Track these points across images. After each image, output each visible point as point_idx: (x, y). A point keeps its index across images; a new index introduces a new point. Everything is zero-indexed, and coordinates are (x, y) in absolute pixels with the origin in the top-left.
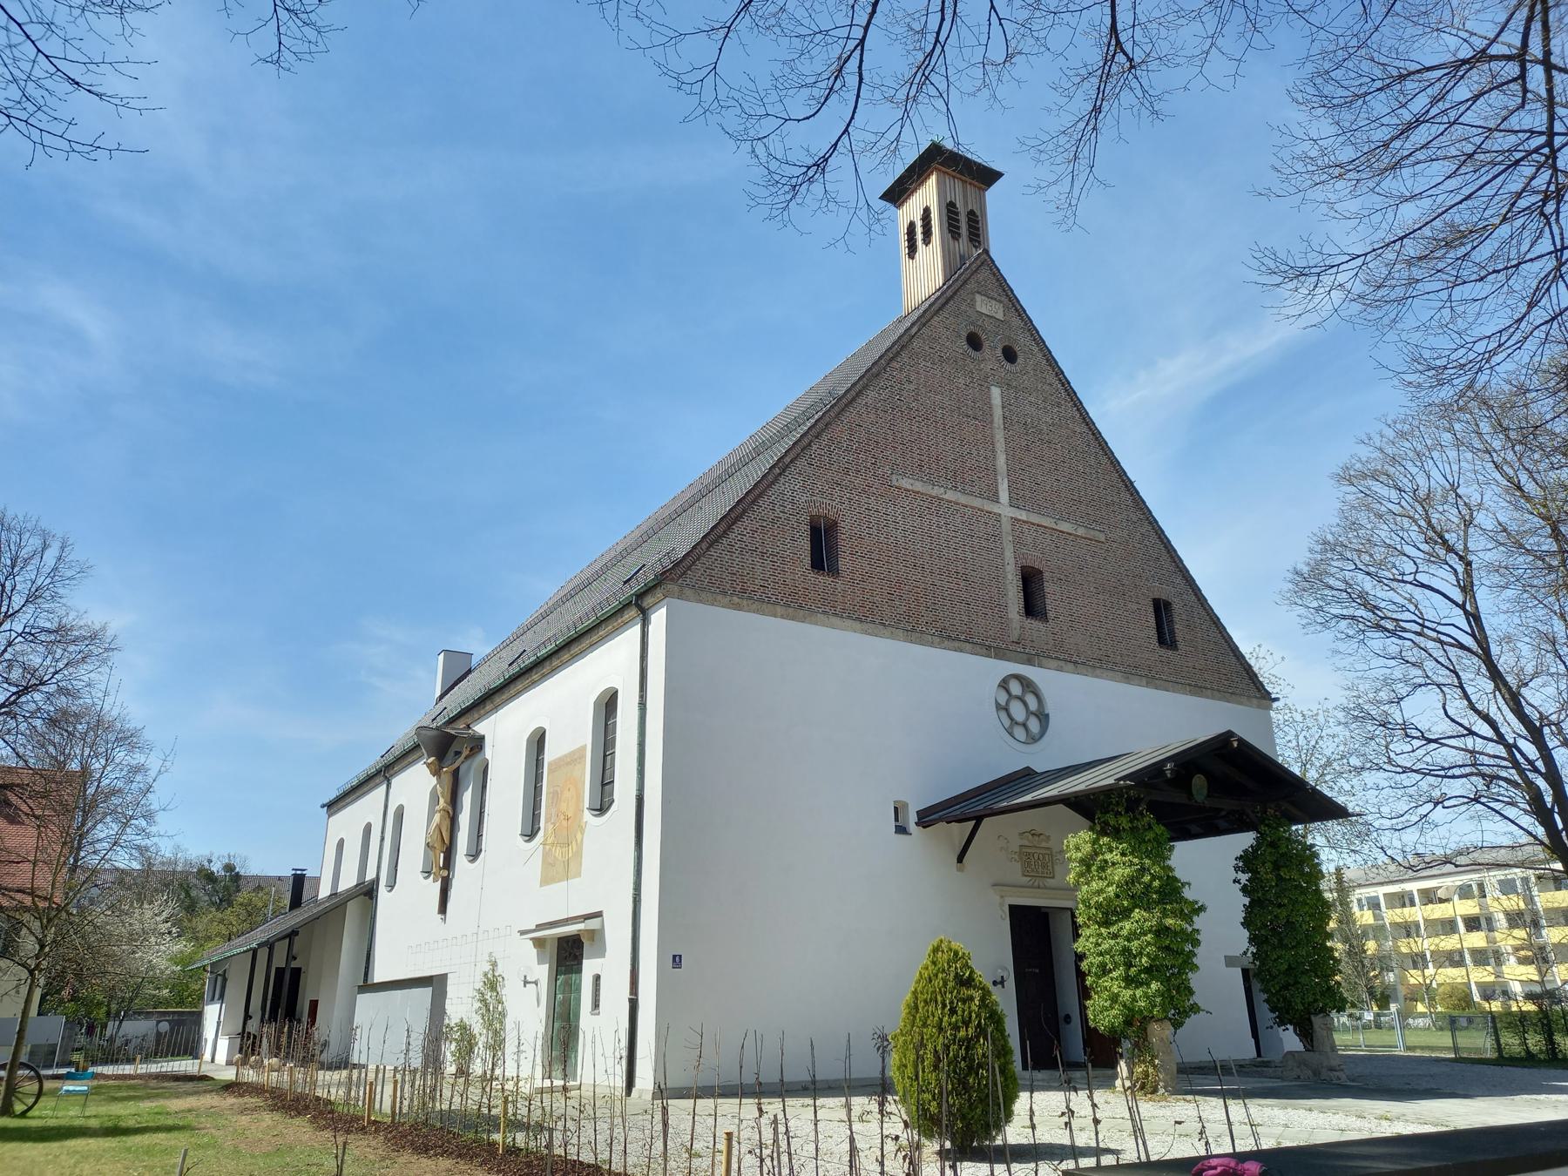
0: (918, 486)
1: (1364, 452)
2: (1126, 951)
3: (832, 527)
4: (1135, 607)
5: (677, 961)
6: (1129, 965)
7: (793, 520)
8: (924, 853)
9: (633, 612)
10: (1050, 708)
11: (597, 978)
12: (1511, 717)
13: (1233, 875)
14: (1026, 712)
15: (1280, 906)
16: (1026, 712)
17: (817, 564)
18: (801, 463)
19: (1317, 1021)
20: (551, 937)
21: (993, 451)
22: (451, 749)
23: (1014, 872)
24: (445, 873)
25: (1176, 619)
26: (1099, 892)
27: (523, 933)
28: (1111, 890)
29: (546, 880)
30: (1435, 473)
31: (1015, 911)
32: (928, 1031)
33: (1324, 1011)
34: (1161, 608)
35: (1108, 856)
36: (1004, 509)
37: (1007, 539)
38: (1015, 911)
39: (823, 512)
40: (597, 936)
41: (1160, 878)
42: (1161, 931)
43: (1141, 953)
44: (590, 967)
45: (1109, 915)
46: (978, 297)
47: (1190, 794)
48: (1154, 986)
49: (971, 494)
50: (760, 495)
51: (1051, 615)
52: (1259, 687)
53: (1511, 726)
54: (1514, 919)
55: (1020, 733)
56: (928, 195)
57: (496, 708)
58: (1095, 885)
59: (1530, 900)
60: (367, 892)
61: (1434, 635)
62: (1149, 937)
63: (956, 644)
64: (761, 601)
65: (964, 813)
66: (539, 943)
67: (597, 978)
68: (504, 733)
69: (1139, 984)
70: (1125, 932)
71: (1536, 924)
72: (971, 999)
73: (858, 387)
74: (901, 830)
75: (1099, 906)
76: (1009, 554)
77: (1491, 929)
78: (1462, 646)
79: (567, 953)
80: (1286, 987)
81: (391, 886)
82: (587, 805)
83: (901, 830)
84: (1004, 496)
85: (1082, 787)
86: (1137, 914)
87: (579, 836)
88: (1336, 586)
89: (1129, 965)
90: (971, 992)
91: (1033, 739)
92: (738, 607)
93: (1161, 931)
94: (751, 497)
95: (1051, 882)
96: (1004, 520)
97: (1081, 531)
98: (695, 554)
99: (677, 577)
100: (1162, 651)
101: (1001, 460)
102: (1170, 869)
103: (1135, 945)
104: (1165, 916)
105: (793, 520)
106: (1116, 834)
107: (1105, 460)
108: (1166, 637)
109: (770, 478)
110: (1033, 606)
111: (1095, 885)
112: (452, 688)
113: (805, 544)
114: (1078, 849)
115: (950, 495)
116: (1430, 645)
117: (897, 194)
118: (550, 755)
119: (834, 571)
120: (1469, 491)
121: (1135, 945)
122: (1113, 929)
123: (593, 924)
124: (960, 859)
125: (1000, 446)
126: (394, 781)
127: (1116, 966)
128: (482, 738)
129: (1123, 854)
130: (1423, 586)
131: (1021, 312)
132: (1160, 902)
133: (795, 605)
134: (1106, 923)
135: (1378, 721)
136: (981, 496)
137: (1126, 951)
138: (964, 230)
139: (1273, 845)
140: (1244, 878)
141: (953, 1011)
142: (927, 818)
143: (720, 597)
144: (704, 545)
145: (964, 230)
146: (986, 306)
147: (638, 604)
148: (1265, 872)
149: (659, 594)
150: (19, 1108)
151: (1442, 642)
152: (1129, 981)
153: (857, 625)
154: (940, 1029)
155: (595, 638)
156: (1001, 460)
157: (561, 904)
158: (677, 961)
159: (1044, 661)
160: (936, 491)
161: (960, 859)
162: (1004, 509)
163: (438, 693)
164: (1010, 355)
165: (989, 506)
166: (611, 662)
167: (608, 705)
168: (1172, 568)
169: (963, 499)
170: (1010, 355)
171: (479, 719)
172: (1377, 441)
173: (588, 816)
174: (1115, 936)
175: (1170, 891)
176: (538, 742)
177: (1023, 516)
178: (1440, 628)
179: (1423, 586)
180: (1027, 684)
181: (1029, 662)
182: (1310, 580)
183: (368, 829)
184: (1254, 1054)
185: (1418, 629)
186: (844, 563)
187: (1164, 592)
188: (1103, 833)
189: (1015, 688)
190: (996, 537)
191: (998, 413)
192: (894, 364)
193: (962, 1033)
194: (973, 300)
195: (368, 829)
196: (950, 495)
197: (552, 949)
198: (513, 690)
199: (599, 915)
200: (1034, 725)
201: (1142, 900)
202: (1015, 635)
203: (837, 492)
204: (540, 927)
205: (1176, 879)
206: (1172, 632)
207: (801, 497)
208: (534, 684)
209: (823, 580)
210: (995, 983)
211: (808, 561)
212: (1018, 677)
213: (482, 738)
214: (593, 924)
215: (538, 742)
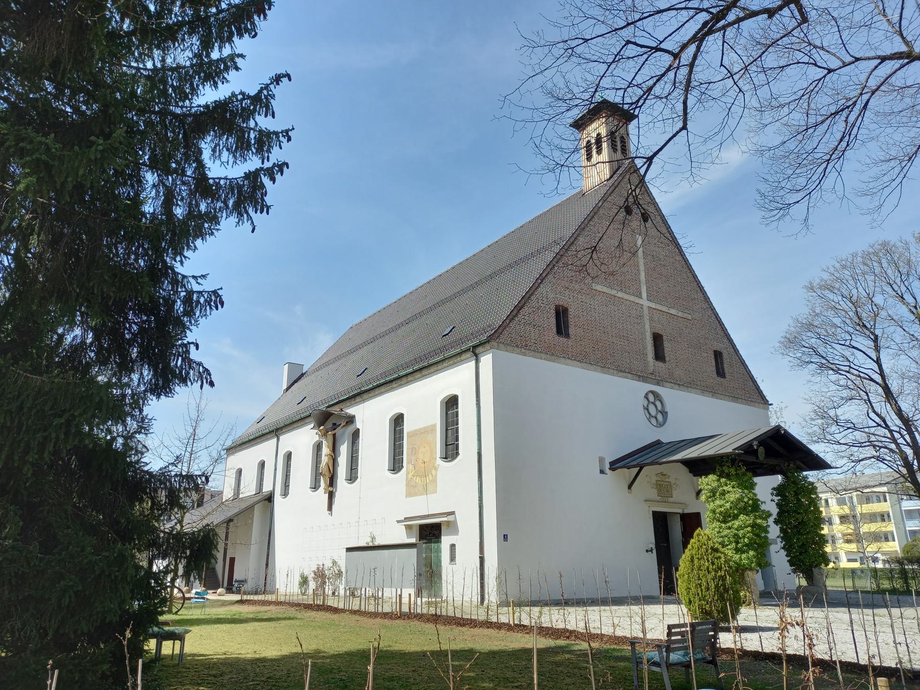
0: (605, 289)
1: (826, 276)
2: (736, 535)
3: (565, 310)
4: (705, 355)
5: (505, 537)
6: (737, 543)
7: (547, 307)
9: (469, 354)
10: (668, 409)
11: (453, 546)
12: (895, 417)
13: (771, 497)
14: (657, 412)
15: (799, 513)
16: (657, 412)
17: (559, 332)
18: (550, 277)
19: (815, 570)
20: (416, 525)
22: (332, 421)
23: (653, 494)
24: (331, 489)
25: (725, 362)
26: (721, 506)
27: (398, 522)
28: (728, 505)
29: (409, 495)
30: (861, 289)
31: (655, 514)
32: (702, 573)
33: (818, 565)
34: (718, 355)
35: (725, 488)
36: (645, 302)
37: (646, 318)
38: (655, 514)
39: (561, 303)
40: (453, 527)
41: (752, 499)
42: (754, 525)
43: (744, 537)
44: (446, 541)
45: (726, 517)
47: (757, 457)
48: (751, 553)
49: (629, 293)
50: (532, 295)
51: (667, 359)
52: (763, 397)
53: (894, 422)
54: (843, 519)
55: (653, 421)
56: (599, 128)
57: (364, 401)
58: (718, 502)
59: (852, 508)
61: (856, 372)
62: (749, 529)
63: (625, 374)
64: (534, 351)
65: (633, 462)
66: (409, 528)
67: (453, 546)
68: (371, 416)
69: (743, 552)
70: (735, 526)
71: (856, 522)
72: (720, 558)
73: (575, 235)
74: (602, 472)
75: (721, 513)
76: (647, 327)
77: (831, 524)
78: (872, 380)
79: (430, 533)
80: (801, 554)
81: (285, 494)
82: (438, 455)
83: (602, 472)
84: (644, 295)
85: (711, 452)
86: (742, 517)
87: (434, 472)
88: (807, 345)
89: (737, 543)
90: (719, 554)
91: (661, 425)
92: (524, 354)
93: (754, 525)
94: (528, 295)
95: (670, 500)
96: (645, 308)
97: (680, 314)
98: (503, 327)
100: (719, 379)
101: (643, 274)
102: (755, 495)
103: (741, 533)
104: (756, 518)
105: (547, 307)
106: (728, 476)
107: (690, 275)
108: (720, 373)
109: (536, 285)
110: (659, 355)
111: (718, 502)
112: (296, 382)
113: (553, 321)
114: (708, 484)
115: (620, 294)
116: (853, 377)
117: (580, 125)
118: (407, 427)
119: (567, 336)
120: (878, 299)
121: (741, 533)
122: (730, 524)
123: (451, 518)
124: (630, 487)
125: (642, 268)
126: (281, 438)
127: (731, 543)
128: (354, 417)
129: (733, 487)
130: (854, 347)
132: (752, 512)
133: (550, 353)
134: (725, 522)
135: (826, 417)
136: (633, 295)
137: (736, 535)
138: (619, 148)
139: (794, 482)
140: (776, 499)
141: (713, 564)
142: (614, 465)
143: (516, 349)
144: (508, 321)
145: (619, 148)
148: (790, 495)
149: (487, 346)
150: (174, 610)
151: (859, 376)
152: (737, 550)
153: (579, 364)
154: (709, 572)
155: (440, 367)
156: (643, 274)
157: (426, 507)
158: (505, 537)
159: (665, 384)
160: (613, 292)
161: (630, 487)
162: (645, 302)
163: (285, 387)
165: (637, 300)
166: (457, 379)
167: (451, 403)
168: (722, 334)
169: (626, 297)
171: (351, 406)
172: (832, 270)
173: (439, 462)
174: (730, 528)
175: (754, 507)
176: (398, 420)
177: (653, 305)
178: (860, 369)
179: (854, 347)
180: (656, 395)
181: (658, 384)
182: (791, 342)
183: (262, 465)
185: (847, 369)
186: (572, 331)
187: (719, 347)
188: (721, 476)
190: (641, 317)
192: (591, 223)
193: (719, 574)
195: (262, 465)
196: (620, 294)
197: (416, 531)
198: (377, 391)
199: (453, 513)
200: (660, 417)
201: (744, 510)
202: (651, 369)
203: (567, 293)
204: (407, 519)
205: (758, 500)
206: (723, 369)
207: (550, 295)
208: (393, 389)
209: (563, 340)
211: (555, 330)
212: (652, 392)
213: (354, 417)
214: (451, 518)
215: (398, 420)
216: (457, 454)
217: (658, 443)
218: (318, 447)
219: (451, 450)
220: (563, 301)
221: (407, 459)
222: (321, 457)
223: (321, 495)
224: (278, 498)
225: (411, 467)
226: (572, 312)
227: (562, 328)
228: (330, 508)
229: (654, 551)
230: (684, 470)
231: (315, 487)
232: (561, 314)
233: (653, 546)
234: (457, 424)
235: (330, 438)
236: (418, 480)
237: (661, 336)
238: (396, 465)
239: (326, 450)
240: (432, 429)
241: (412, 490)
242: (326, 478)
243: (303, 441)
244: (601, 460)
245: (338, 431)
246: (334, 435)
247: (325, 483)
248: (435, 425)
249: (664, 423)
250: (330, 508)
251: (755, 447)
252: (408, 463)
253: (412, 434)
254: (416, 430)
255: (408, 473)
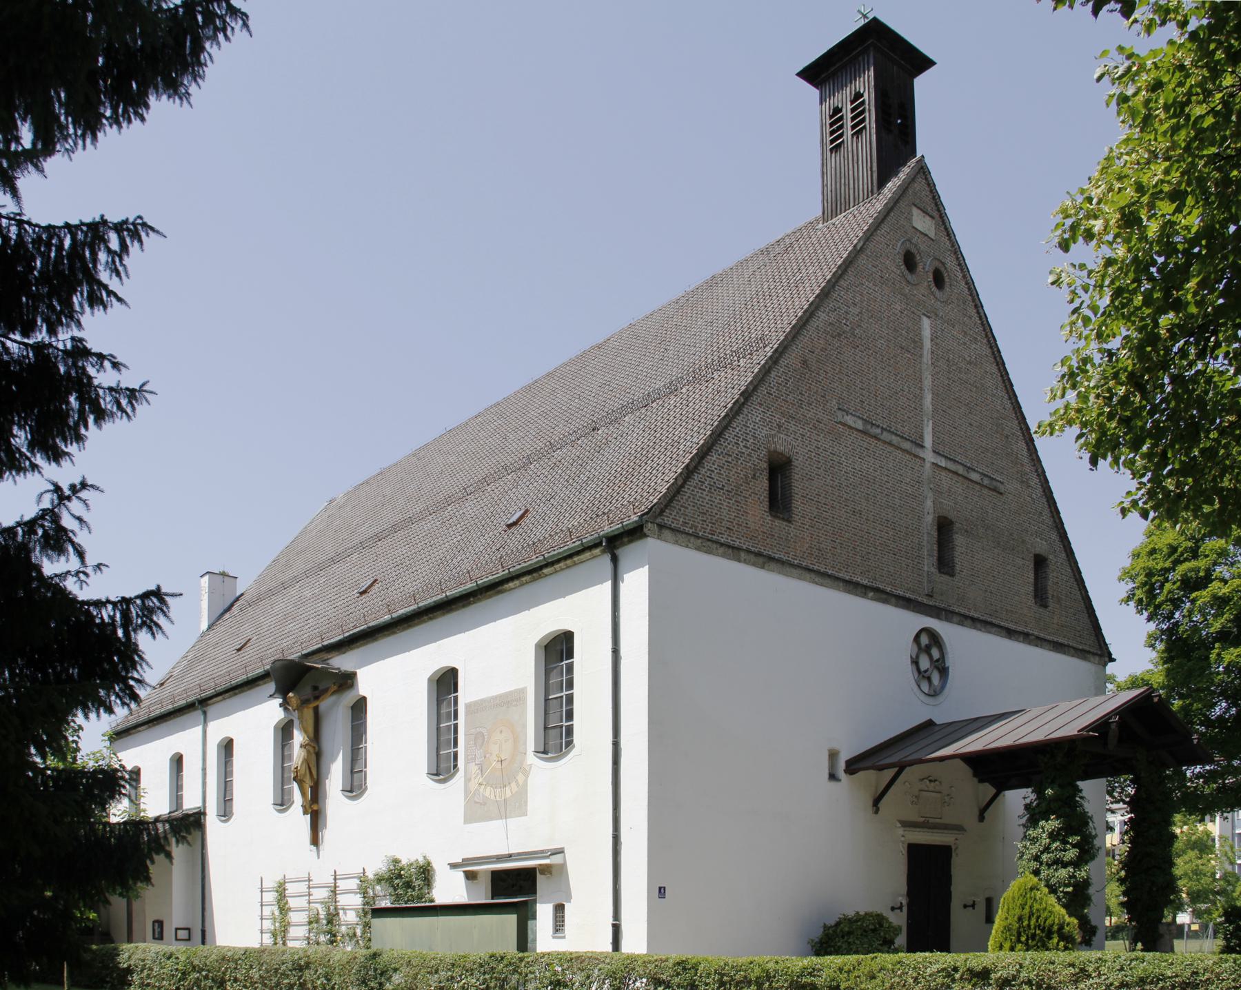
5: (662, 891)
8: (847, 796)
10: (950, 662)
14: (930, 660)
20: (486, 871)
21: (921, 389)
27: (454, 866)
29: (469, 819)
34: (1040, 562)
40: (556, 872)
46: (915, 211)
60: (188, 826)
66: (470, 876)
76: (929, 503)
81: (226, 812)
82: (531, 746)
83: (833, 777)
87: (520, 778)
91: (934, 694)
99: (660, 520)
101: (928, 399)
118: (467, 693)
131: (949, 233)
142: (853, 766)
146: (922, 223)
147: (615, 544)
156: (928, 399)
157: (506, 840)
158: (662, 891)
164: (939, 279)
166: (579, 608)
167: (558, 648)
170: (939, 279)
173: (532, 759)
180: (935, 639)
184: (608, 948)
186: (798, 505)
187: (1041, 547)
189: (925, 640)
191: (927, 344)
194: (910, 213)
199: (560, 851)
204: (467, 862)
207: (760, 426)
210: (893, 909)
214: (556, 860)
216: (570, 743)
217: (929, 724)
218: (284, 732)
219: (556, 735)
220: (782, 444)
221: (466, 756)
222: (291, 748)
223: (297, 818)
224: (212, 822)
225: (474, 768)
226: (799, 462)
227: (779, 502)
228: (315, 841)
229: (905, 909)
230: (965, 770)
231: (282, 803)
232: (779, 469)
233: (904, 902)
234: (570, 685)
235: (309, 713)
236: (488, 792)
237: (951, 523)
238: (442, 766)
239: (298, 738)
240: (511, 700)
241: (476, 811)
242: (306, 785)
243: (257, 723)
244: (833, 755)
245: (324, 704)
246: (316, 710)
247: (303, 794)
248: (523, 691)
249: (943, 687)
250: (315, 841)
251: (61, 766)
252: (467, 762)
253: (468, 706)
254: (483, 701)
255: (467, 780)
